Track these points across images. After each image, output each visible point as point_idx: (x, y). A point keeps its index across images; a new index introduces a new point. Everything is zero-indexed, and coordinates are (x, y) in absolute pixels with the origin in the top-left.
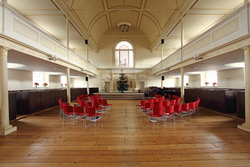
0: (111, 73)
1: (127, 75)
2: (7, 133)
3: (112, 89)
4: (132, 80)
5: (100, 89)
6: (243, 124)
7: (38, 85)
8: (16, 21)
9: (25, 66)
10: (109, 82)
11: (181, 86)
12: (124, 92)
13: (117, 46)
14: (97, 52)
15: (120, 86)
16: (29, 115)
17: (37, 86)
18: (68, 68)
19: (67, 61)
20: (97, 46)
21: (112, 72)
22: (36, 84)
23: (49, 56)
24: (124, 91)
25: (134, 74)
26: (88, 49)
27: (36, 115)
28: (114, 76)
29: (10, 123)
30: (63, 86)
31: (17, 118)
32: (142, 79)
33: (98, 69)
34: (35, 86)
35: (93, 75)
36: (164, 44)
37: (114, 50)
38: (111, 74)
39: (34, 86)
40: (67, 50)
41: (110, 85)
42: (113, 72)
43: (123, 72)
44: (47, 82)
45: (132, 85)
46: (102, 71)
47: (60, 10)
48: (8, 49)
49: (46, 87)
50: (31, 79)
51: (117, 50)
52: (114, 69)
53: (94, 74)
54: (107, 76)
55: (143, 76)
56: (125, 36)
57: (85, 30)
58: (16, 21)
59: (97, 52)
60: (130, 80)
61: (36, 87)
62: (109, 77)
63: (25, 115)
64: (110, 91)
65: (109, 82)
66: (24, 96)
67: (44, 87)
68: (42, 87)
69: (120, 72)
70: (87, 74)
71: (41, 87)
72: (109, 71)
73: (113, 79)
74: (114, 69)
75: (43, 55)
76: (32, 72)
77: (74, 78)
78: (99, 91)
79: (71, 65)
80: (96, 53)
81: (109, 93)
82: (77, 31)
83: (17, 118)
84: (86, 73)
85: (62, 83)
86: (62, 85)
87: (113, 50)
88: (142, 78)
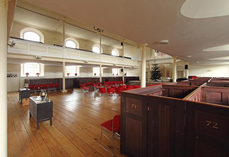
0: (149, 64)
1: (164, 64)
2: (63, 92)
4: (168, 70)
12: (157, 81)
14: (138, 48)
22: (95, 74)
23: (84, 61)
24: (157, 80)
25: (171, 63)
32: (180, 68)
33: (139, 61)
36: (28, 73)
39: (94, 75)
43: (156, 63)
45: (169, 73)
50: (92, 72)
55: (181, 65)
59: (138, 48)
60: (167, 70)
61: (38, 76)
69: (154, 63)
71: (115, 75)
74: (151, 60)
76: (92, 68)
79: (101, 63)
80: (137, 49)
85: (113, 73)
86: (113, 74)
88: (180, 66)
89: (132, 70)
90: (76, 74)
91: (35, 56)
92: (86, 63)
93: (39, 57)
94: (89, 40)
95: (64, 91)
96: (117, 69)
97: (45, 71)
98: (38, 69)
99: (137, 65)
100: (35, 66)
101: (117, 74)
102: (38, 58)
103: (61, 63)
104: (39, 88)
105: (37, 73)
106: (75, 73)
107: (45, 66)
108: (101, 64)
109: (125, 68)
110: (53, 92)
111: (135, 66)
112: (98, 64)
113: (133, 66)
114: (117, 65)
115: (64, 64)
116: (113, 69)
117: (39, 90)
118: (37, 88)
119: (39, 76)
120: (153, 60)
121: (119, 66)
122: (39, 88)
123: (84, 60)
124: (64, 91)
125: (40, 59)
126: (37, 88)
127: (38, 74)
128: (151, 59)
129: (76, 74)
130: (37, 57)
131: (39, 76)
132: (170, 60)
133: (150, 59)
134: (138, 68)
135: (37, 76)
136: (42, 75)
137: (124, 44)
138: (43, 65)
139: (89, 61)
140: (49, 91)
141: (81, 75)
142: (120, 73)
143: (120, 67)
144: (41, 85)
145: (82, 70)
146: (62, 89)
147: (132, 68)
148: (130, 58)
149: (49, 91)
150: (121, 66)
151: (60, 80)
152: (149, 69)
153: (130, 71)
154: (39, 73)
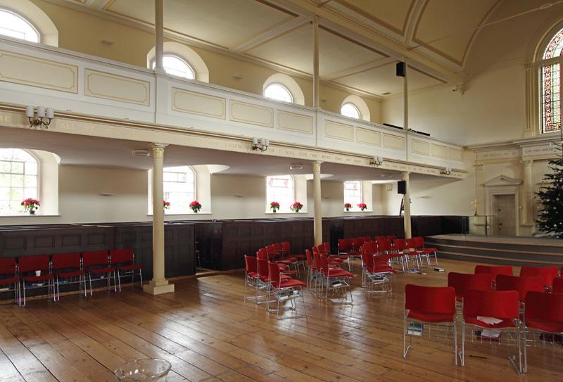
0: (520, 158)
2: (157, 291)
3: (524, 222)
5: (473, 221)
6: (150, 282)
7: (278, 208)
8: (177, 92)
9: (229, 167)
10: (514, 195)
11: (151, 212)
13: (551, 44)
14: (463, 90)
15: (551, 211)
16: (221, 272)
17: (277, 209)
18: (406, 172)
19: (404, 160)
20: (461, 69)
21: (524, 154)
22: (275, 205)
23: (251, 141)
26: (409, 89)
27: (226, 274)
28: (530, 170)
29: (166, 276)
30: (350, 210)
31: (197, 274)
33: (465, 148)
34: (272, 209)
35: (437, 173)
37: (533, 68)
38: (519, 164)
39: (269, 210)
40: (404, 136)
41: (514, 207)
42: (529, 154)
44: (303, 201)
46: (481, 154)
47: (297, 16)
48: (162, 145)
49: (300, 211)
50: (260, 194)
51: (551, 62)
52: (532, 142)
53: (443, 171)
54: (504, 174)
56: (551, 5)
57: (393, 34)
58: (177, 92)
59: (463, 90)
61: (32, 212)
62: (510, 174)
63: (217, 269)
64: (514, 228)
65: (514, 195)
66: (216, 232)
67: (295, 212)
68: (291, 211)
70: (400, 172)
71: (286, 210)
72: (511, 154)
73: (530, 181)
74: (532, 142)
75: (235, 143)
76: (263, 178)
77: (388, 184)
78: (472, 228)
80: (458, 93)
81: (514, 236)
82: (361, 47)
83: (197, 274)
84: (402, 170)
85: (346, 201)
87: (528, 65)
89: (430, 187)
90: (196, 206)
91: (21, 110)
92: (258, 152)
93: (42, 114)
94: (249, 53)
95: (162, 286)
96: (196, 174)
97: (65, 189)
98: (33, 182)
99: (459, 165)
100: (180, 178)
101: (364, 206)
102: (36, 123)
103: (145, 149)
104: (38, 273)
105: (26, 198)
106: (192, 200)
107: (61, 166)
108: (320, 158)
109: (413, 175)
110: (104, 293)
111: (453, 167)
112: (308, 156)
113: (448, 167)
114: (384, 166)
115: (160, 154)
116: (268, 178)
117: (37, 282)
118: (28, 276)
119: (37, 213)
120: (551, 141)
121: (391, 167)
122: (38, 273)
123: (251, 136)
124: (162, 286)
125: (47, 125)
126: (28, 276)
127: (30, 203)
128: (533, 135)
129: (196, 206)
130: (31, 114)
131: (37, 213)
132: (532, 148)
133: (527, 136)
134: (463, 176)
135: (28, 214)
136: (50, 208)
137: (408, 71)
138: (53, 161)
139: (272, 143)
140: (88, 288)
141: (215, 209)
142: (374, 200)
143: (389, 174)
144: (51, 258)
145: (221, 187)
146: (149, 276)
147: (442, 177)
148: (429, 135)
149: (88, 288)
150: (398, 168)
151: (137, 234)
152: (522, 183)
153: (424, 194)
154: (34, 197)
